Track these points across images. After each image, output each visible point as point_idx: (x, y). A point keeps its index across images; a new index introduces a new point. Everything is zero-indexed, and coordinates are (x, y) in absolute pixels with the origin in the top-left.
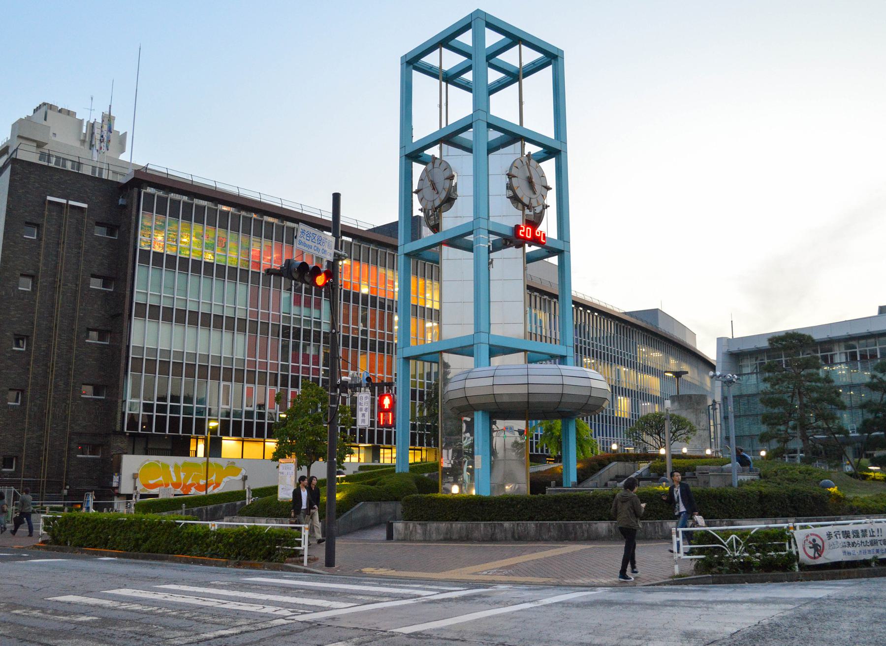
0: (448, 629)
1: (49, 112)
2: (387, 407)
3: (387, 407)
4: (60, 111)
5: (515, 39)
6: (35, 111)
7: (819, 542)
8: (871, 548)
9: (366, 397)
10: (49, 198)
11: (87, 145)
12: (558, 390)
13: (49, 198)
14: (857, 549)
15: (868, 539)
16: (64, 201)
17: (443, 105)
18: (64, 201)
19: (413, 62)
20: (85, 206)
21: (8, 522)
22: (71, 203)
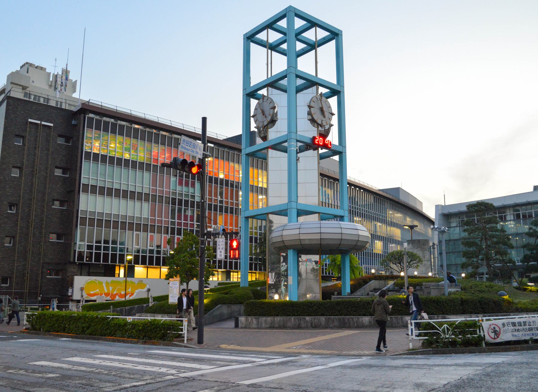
0: (272, 382)
1: (30, 68)
2: (235, 247)
3: (235, 247)
4: (37, 67)
5: (312, 23)
6: (21, 67)
7: (497, 329)
8: (529, 332)
9: (222, 241)
10: (30, 120)
11: (53, 88)
12: (339, 237)
13: (30, 120)
14: (521, 333)
15: (527, 327)
16: (39, 122)
17: (269, 64)
18: (39, 122)
19: (251, 37)
20: (52, 125)
22: (43, 123)
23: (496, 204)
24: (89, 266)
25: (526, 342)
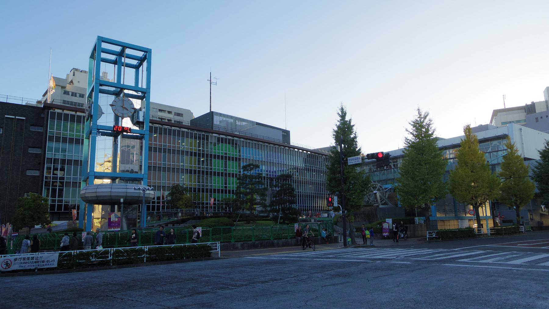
0: (531, 255)
1: (76, 72)
7: (9, 262)
8: (35, 264)
10: (6, 116)
12: (109, 194)
13: (6, 116)
14: (27, 265)
15: (34, 260)
16: (14, 117)
18: (14, 117)
20: (24, 118)
21: (27, 238)
22: (17, 117)
23: (393, 155)
24: (59, 213)
25: (33, 270)
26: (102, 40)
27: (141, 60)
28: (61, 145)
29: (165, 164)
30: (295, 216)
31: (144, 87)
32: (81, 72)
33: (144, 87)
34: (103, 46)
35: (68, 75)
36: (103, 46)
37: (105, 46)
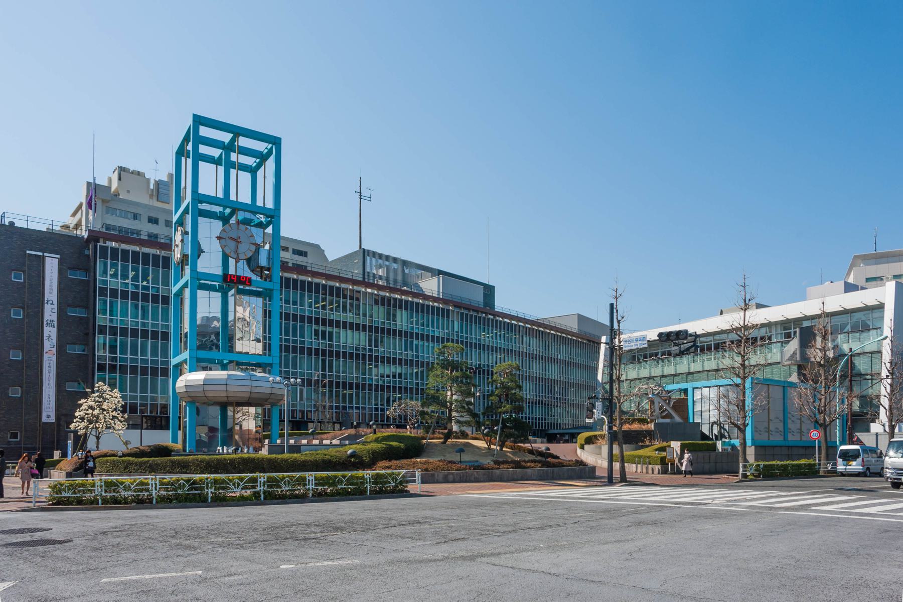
10: (28, 252)
13: (28, 252)
16: (41, 254)
18: (41, 254)
26: (199, 121)
27: (263, 158)
28: (328, 329)
29: (331, 346)
30: (762, 463)
31: (270, 204)
32: (132, 173)
33: (270, 204)
34: (201, 134)
35: (110, 180)
36: (201, 134)
37: (204, 131)
